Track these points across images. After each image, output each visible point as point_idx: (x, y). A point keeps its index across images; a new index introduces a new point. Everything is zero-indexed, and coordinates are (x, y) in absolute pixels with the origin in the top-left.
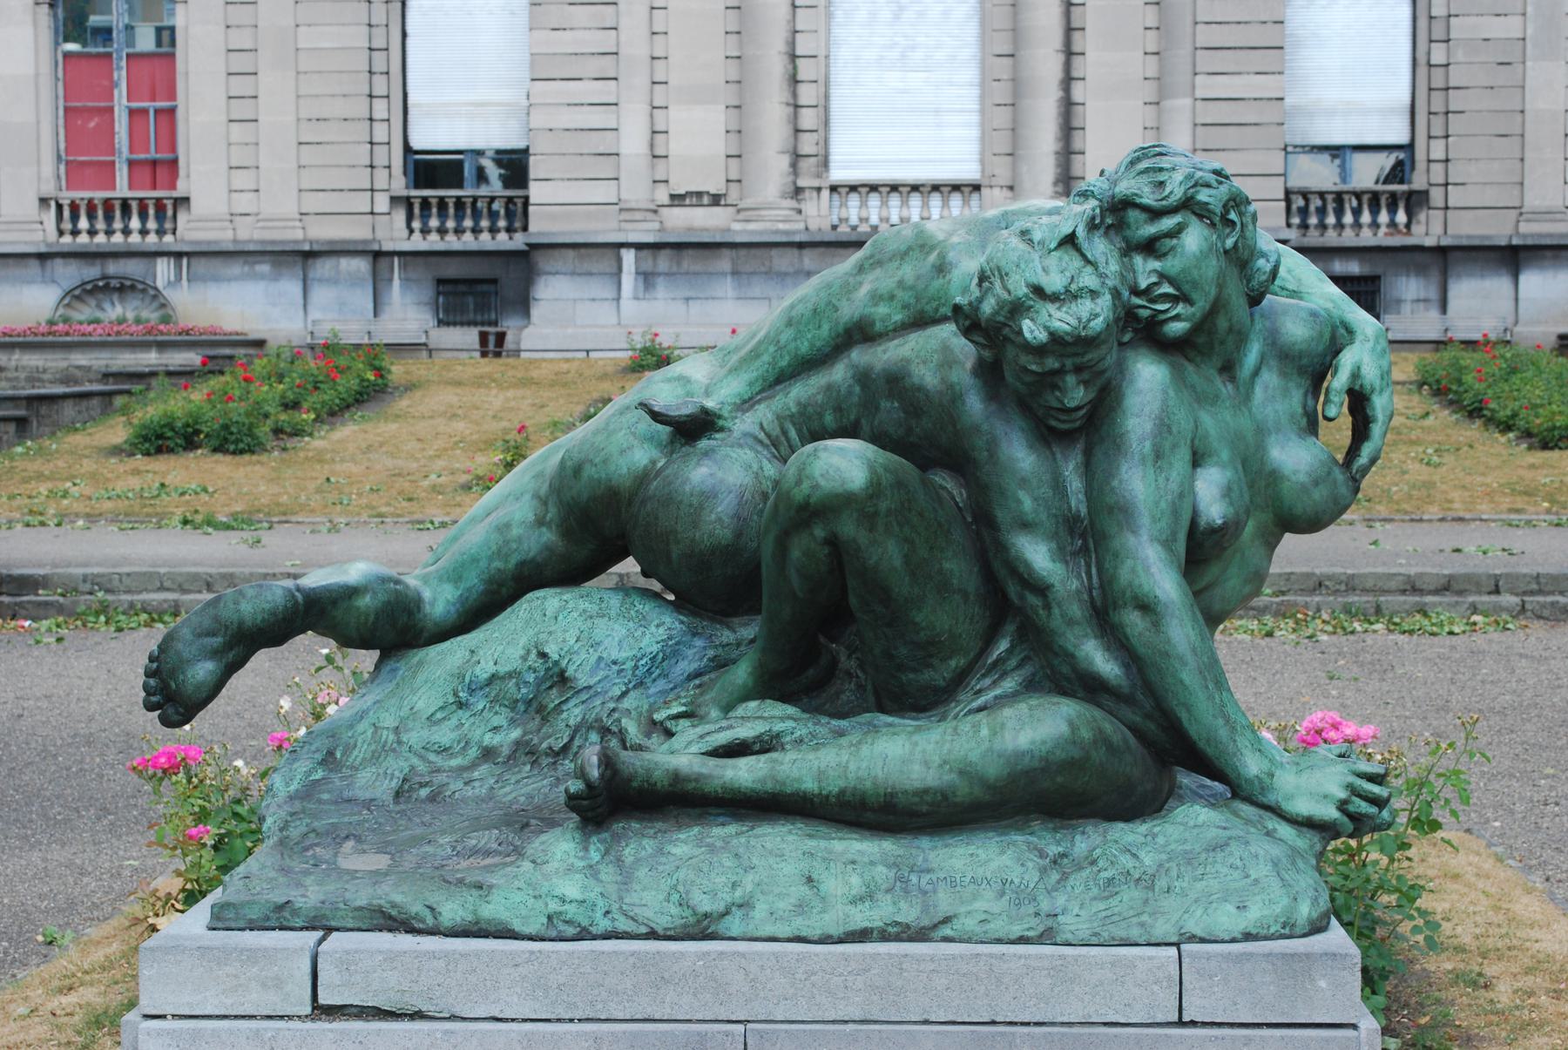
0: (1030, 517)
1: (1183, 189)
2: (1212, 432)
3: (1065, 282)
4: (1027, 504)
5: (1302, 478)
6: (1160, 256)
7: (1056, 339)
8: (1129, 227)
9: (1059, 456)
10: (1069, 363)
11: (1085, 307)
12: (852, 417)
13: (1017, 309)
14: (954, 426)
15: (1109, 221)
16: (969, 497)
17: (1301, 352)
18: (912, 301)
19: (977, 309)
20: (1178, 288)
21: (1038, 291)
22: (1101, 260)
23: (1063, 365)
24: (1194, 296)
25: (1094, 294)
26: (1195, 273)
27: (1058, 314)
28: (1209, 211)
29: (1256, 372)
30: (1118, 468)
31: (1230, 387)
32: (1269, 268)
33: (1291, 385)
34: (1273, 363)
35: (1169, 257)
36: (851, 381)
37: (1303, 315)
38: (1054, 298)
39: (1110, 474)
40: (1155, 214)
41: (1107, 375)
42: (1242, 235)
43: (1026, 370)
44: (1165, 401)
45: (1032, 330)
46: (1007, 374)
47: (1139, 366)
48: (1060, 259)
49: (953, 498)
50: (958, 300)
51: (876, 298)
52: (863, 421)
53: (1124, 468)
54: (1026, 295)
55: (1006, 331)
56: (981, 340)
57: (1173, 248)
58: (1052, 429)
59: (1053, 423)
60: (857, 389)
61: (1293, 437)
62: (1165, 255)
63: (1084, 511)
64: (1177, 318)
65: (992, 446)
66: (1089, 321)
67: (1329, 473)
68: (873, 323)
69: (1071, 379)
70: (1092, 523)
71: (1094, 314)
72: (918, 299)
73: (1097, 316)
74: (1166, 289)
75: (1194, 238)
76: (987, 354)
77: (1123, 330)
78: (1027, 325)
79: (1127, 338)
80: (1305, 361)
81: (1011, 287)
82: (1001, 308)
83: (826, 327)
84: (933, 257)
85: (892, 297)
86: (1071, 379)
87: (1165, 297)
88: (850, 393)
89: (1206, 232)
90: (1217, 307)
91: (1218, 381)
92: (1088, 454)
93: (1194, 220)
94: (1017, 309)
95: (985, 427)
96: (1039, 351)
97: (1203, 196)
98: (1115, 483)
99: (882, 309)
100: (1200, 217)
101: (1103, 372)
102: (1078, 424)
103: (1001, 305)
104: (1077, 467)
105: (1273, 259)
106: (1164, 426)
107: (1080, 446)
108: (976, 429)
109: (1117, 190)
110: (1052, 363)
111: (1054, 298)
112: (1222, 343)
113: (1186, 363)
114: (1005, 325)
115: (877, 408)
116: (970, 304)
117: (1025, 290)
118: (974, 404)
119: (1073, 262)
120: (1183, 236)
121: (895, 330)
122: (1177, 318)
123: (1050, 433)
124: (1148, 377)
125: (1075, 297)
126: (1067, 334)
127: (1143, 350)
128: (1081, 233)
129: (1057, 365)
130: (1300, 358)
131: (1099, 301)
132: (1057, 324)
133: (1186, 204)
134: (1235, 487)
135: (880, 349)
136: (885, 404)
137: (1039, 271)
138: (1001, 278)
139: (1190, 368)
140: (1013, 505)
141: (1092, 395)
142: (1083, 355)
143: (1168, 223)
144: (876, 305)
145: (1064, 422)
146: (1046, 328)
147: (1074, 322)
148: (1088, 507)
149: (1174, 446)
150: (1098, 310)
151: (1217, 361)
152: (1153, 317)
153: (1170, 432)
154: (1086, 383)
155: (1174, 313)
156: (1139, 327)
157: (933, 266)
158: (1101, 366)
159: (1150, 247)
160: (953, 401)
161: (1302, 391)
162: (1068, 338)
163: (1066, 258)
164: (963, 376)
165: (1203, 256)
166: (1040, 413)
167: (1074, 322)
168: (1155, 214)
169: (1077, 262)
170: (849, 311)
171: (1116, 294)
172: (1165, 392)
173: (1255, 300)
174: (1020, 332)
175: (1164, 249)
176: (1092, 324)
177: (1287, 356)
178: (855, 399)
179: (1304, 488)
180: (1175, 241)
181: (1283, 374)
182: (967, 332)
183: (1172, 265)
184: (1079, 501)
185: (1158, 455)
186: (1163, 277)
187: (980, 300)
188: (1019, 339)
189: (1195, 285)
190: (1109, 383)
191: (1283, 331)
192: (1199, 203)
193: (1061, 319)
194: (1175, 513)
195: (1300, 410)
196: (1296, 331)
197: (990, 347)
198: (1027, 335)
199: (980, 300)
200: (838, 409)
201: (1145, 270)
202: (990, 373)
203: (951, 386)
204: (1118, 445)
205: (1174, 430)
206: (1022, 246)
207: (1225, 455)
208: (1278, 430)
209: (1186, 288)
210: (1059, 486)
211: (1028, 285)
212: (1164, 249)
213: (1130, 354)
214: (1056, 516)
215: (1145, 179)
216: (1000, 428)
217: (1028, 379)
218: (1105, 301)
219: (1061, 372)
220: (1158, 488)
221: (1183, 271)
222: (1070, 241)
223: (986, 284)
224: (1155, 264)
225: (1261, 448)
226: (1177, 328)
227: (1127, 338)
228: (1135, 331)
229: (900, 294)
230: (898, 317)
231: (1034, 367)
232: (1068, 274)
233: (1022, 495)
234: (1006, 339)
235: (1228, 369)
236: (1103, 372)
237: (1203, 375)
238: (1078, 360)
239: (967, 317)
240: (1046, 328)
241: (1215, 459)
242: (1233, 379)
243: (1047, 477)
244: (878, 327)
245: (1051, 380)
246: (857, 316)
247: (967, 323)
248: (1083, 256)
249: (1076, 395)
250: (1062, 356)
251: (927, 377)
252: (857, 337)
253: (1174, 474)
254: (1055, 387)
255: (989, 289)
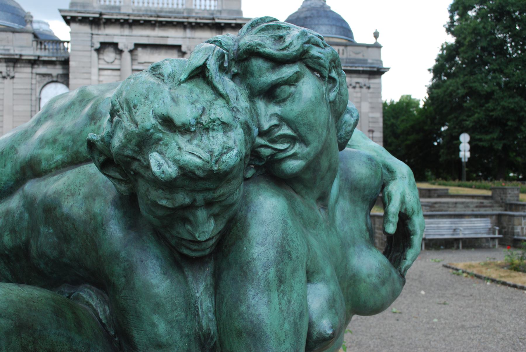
0: (164, 340)
1: (300, 42)
2: (319, 253)
3: (196, 114)
4: (162, 328)
5: (374, 280)
6: (280, 101)
7: (187, 176)
8: (252, 75)
9: (190, 279)
10: (200, 198)
11: (217, 140)
12: (23, 238)
13: (144, 142)
14: (97, 252)
15: (234, 70)
16: (111, 314)
17: (365, 185)
18: (70, 144)
19: (109, 144)
20: (295, 130)
21: (167, 122)
22: (232, 96)
23: (194, 201)
24: (310, 137)
25: (226, 126)
26: (311, 117)
27: (189, 147)
28: (321, 65)
29: (336, 202)
30: (245, 294)
31: (323, 212)
32: (352, 121)
33: (358, 209)
34: (346, 193)
35: (288, 103)
36: (22, 209)
37: (364, 159)
38: (184, 130)
39: (238, 301)
40: (277, 62)
41: (235, 208)
42: (339, 93)
43: (155, 204)
44: (285, 232)
45: (160, 164)
46: (142, 207)
47: (261, 198)
48: (191, 91)
49: (97, 315)
50: (90, 136)
51: (44, 142)
52: (32, 242)
53: (251, 293)
54: (154, 127)
55: (135, 165)
56: (117, 175)
57: (291, 95)
58: (185, 257)
59: (185, 251)
60: (27, 215)
61: (365, 248)
62: (284, 100)
63: (213, 329)
64: (294, 156)
65: (130, 271)
66: (221, 154)
67: (390, 274)
68: (40, 162)
69: (202, 214)
70: (222, 344)
71: (225, 147)
72: (74, 142)
73: (229, 149)
74: (285, 130)
75: (309, 87)
76: (123, 188)
77: (247, 168)
78: (155, 160)
79: (250, 174)
80: (367, 192)
81: (138, 119)
82: (129, 141)
83: (9, 166)
84: (88, 109)
85: (55, 141)
86: (202, 214)
87: (285, 138)
88: (21, 218)
89: (318, 83)
90: (325, 149)
91: (316, 208)
92: (217, 277)
93: (307, 71)
94: (144, 142)
95: (123, 254)
96: (169, 186)
97: (315, 51)
98: (243, 308)
99: (47, 151)
100: (313, 70)
101: (232, 205)
102: (207, 252)
103: (129, 137)
104: (207, 288)
105: (355, 115)
106: (284, 253)
107: (209, 269)
108: (115, 256)
109: (242, 42)
110: (182, 198)
111: (184, 130)
112: (322, 179)
113: (295, 195)
114: (134, 159)
115: (39, 233)
116: (102, 139)
117: (154, 121)
118: (115, 231)
119: (202, 94)
120: (300, 84)
121: (57, 168)
122: (294, 156)
123: (181, 259)
124: (268, 208)
125: (207, 129)
126: (199, 168)
127: (263, 185)
128: (212, 66)
129: (188, 201)
130: (364, 190)
131: (231, 134)
132: (187, 158)
133: (302, 57)
134: (337, 298)
135: (43, 183)
136: (43, 230)
137: (168, 101)
138: (130, 110)
139: (298, 199)
140: (148, 328)
141: (221, 227)
142: (214, 190)
143: (287, 71)
144: (43, 147)
145: (195, 250)
146: (176, 162)
147: (206, 156)
148: (217, 325)
149: (294, 270)
150: (231, 143)
151: (316, 193)
152: (272, 155)
153: (290, 258)
154: (216, 216)
155: (291, 152)
156: (263, 167)
157: (87, 115)
158: (230, 200)
159: (271, 93)
160: (96, 230)
161: (364, 214)
162: (200, 173)
163: (197, 90)
164: (105, 208)
165: (315, 104)
166: (173, 242)
167: (206, 156)
168: (277, 62)
169: (208, 95)
170: (25, 151)
171: (247, 129)
172: (285, 222)
173: (342, 147)
174: (148, 167)
175: (283, 96)
176: (225, 158)
177: (356, 188)
178: (25, 224)
179: (376, 288)
180: (293, 89)
181: (353, 202)
182: (103, 167)
183: (291, 109)
184: (210, 320)
185: (281, 280)
186: (283, 120)
187: (111, 135)
188: (147, 174)
189: (311, 127)
190: (236, 214)
191: (353, 170)
192: (312, 57)
193: (192, 152)
194: (297, 332)
195: (364, 227)
196: (360, 171)
197: (126, 182)
198: (155, 168)
199: (111, 135)
200: (13, 231)
201: (268, 113)
202: (128, 204)
203: (94, 217)
204: (245, 271)
205: (294, 256)
206: (152, 79)
207: (328, 271)
208: (354, 244)
209: (303, 130)
210: (191, 307)
211: (156, 116)
212: (283, 96)
213: (252, 188)
214: (188, 335)
215: (266, 34)
216: (136, 254)
217: (160, 213)
218: (237, 136)
219: (192, 207)
220: (281, 310)
221: (301, 114)
222: (200, 73)
223: (116, 118)
224: (276, 109)
225: (345, 258)
226: (293, 165)
227: (250, 173)
228: (257, 167)
229: (60, 138)
230: (59, 157)
231: (164, 202)
232: (199, 106)
233: (155, 318)
234: (137, 174)
235: (323, 199)
236: (232, 205)
237: (307, 204)
238: (209, 195)
239: (101, 153)
240: (176, 162)
241: (322, 275)
242: (325, 207)
243: (179, 301)
244: (44, 165)
245: (182, 215)
246: (28, 156)
247: (102, 159)
248: (215, 89)
249: (207, 228)
250: (192, 191)
251: (73, 207)
252: (29, 173)
253: (295, 296)
254: (186, 221)
255: (118, 122)
